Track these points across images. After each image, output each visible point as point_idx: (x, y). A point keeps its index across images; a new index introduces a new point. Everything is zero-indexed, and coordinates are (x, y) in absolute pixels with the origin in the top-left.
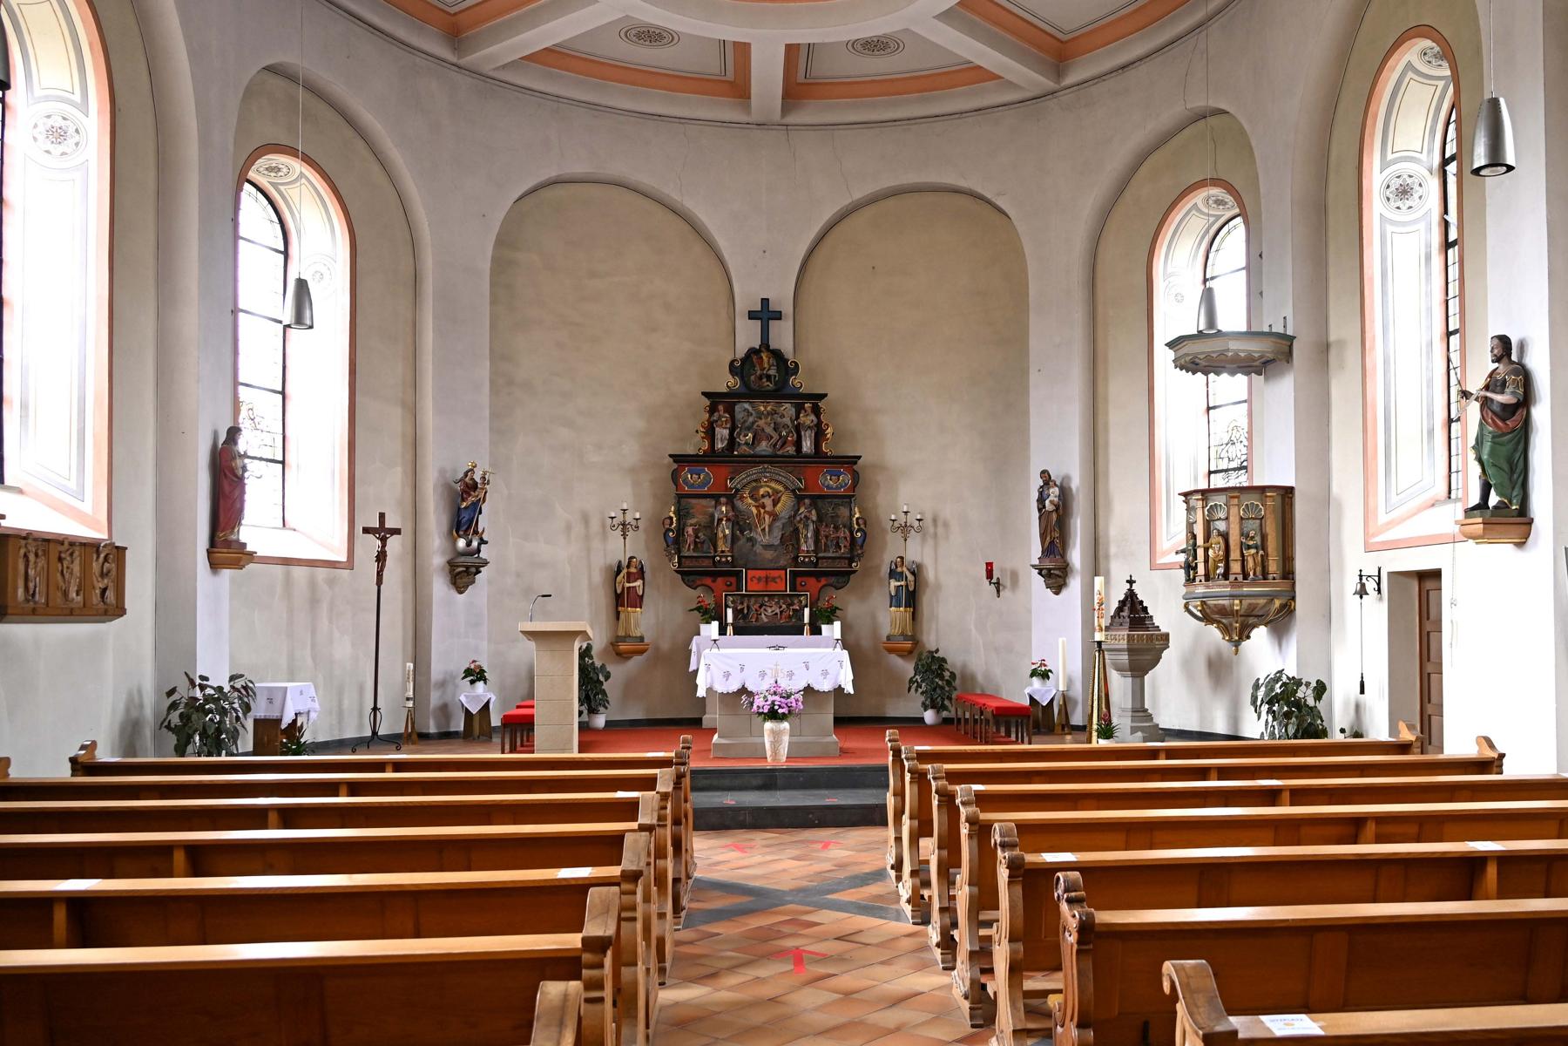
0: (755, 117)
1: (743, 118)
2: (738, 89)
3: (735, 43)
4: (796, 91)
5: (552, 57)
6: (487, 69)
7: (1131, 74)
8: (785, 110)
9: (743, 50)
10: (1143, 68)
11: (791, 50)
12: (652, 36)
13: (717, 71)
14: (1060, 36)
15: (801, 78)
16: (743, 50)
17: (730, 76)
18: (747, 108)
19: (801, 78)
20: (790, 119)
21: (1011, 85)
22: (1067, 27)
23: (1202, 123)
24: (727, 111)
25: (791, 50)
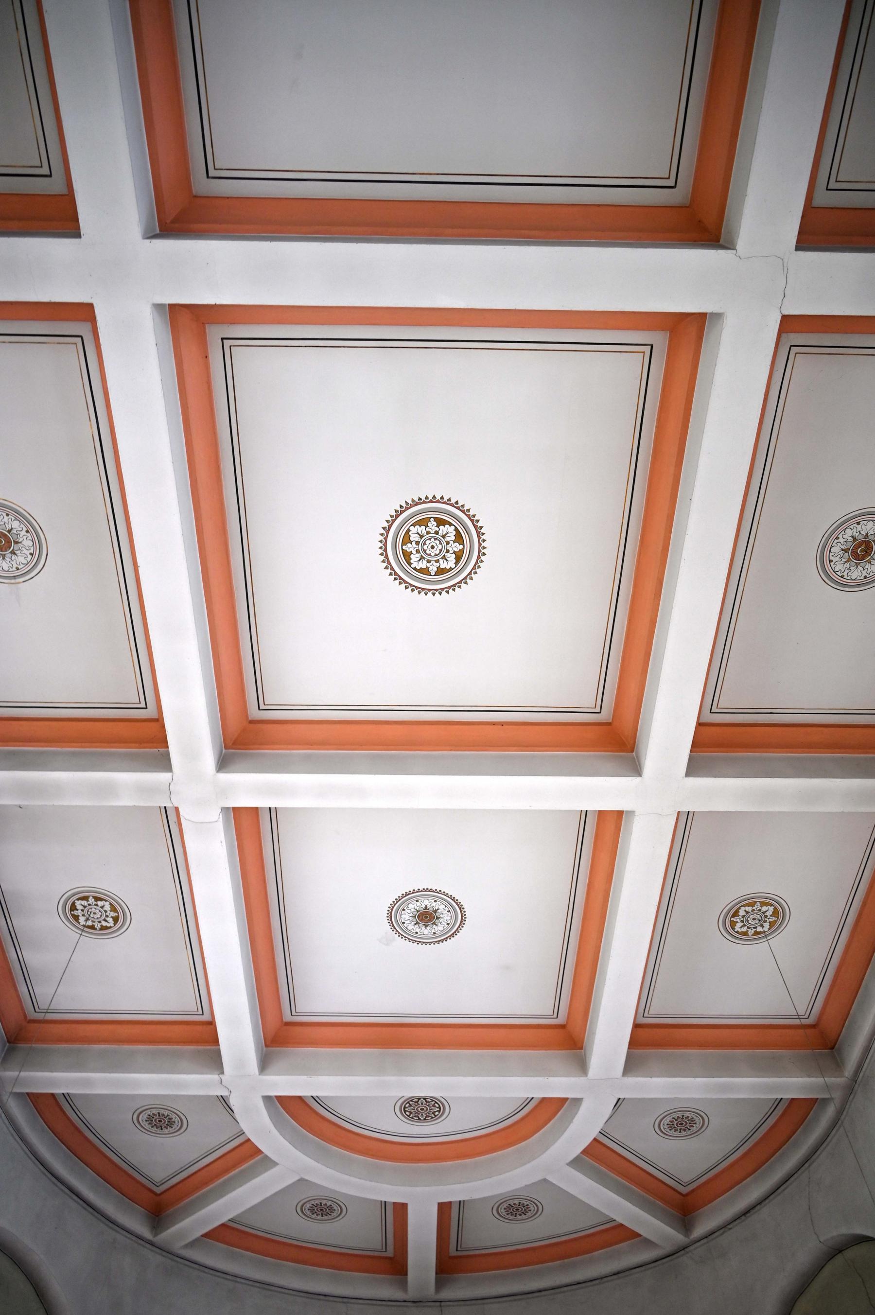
0: (412, 1293)
1: (399, 1295)
2: (395, 1265)
3: (394, 1203)
4: (450, 1263)
5: (228, 1234)
6: (177, 1247)
7: (754, 1218)
8: (440, 1284)
9: (401, 1209)
10: (765, 1212)
11: (444, 1208)
12: (323, 1208)
13: (378, 1246)
14: (680, 1188)
15: (453, 1252)
16: (401, 1209)
17: (390, 1253)
18: (404, 1286)
19: (453, 1252)
20: (447, 1294)
21: (648, 1243)
22: (686, 1179)
23: (839, 1259)
24: (387, 1291)
25: (444, 1208)
